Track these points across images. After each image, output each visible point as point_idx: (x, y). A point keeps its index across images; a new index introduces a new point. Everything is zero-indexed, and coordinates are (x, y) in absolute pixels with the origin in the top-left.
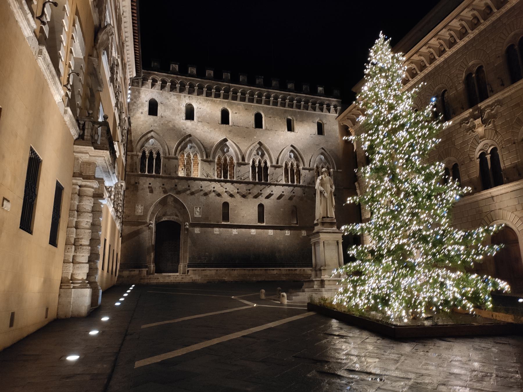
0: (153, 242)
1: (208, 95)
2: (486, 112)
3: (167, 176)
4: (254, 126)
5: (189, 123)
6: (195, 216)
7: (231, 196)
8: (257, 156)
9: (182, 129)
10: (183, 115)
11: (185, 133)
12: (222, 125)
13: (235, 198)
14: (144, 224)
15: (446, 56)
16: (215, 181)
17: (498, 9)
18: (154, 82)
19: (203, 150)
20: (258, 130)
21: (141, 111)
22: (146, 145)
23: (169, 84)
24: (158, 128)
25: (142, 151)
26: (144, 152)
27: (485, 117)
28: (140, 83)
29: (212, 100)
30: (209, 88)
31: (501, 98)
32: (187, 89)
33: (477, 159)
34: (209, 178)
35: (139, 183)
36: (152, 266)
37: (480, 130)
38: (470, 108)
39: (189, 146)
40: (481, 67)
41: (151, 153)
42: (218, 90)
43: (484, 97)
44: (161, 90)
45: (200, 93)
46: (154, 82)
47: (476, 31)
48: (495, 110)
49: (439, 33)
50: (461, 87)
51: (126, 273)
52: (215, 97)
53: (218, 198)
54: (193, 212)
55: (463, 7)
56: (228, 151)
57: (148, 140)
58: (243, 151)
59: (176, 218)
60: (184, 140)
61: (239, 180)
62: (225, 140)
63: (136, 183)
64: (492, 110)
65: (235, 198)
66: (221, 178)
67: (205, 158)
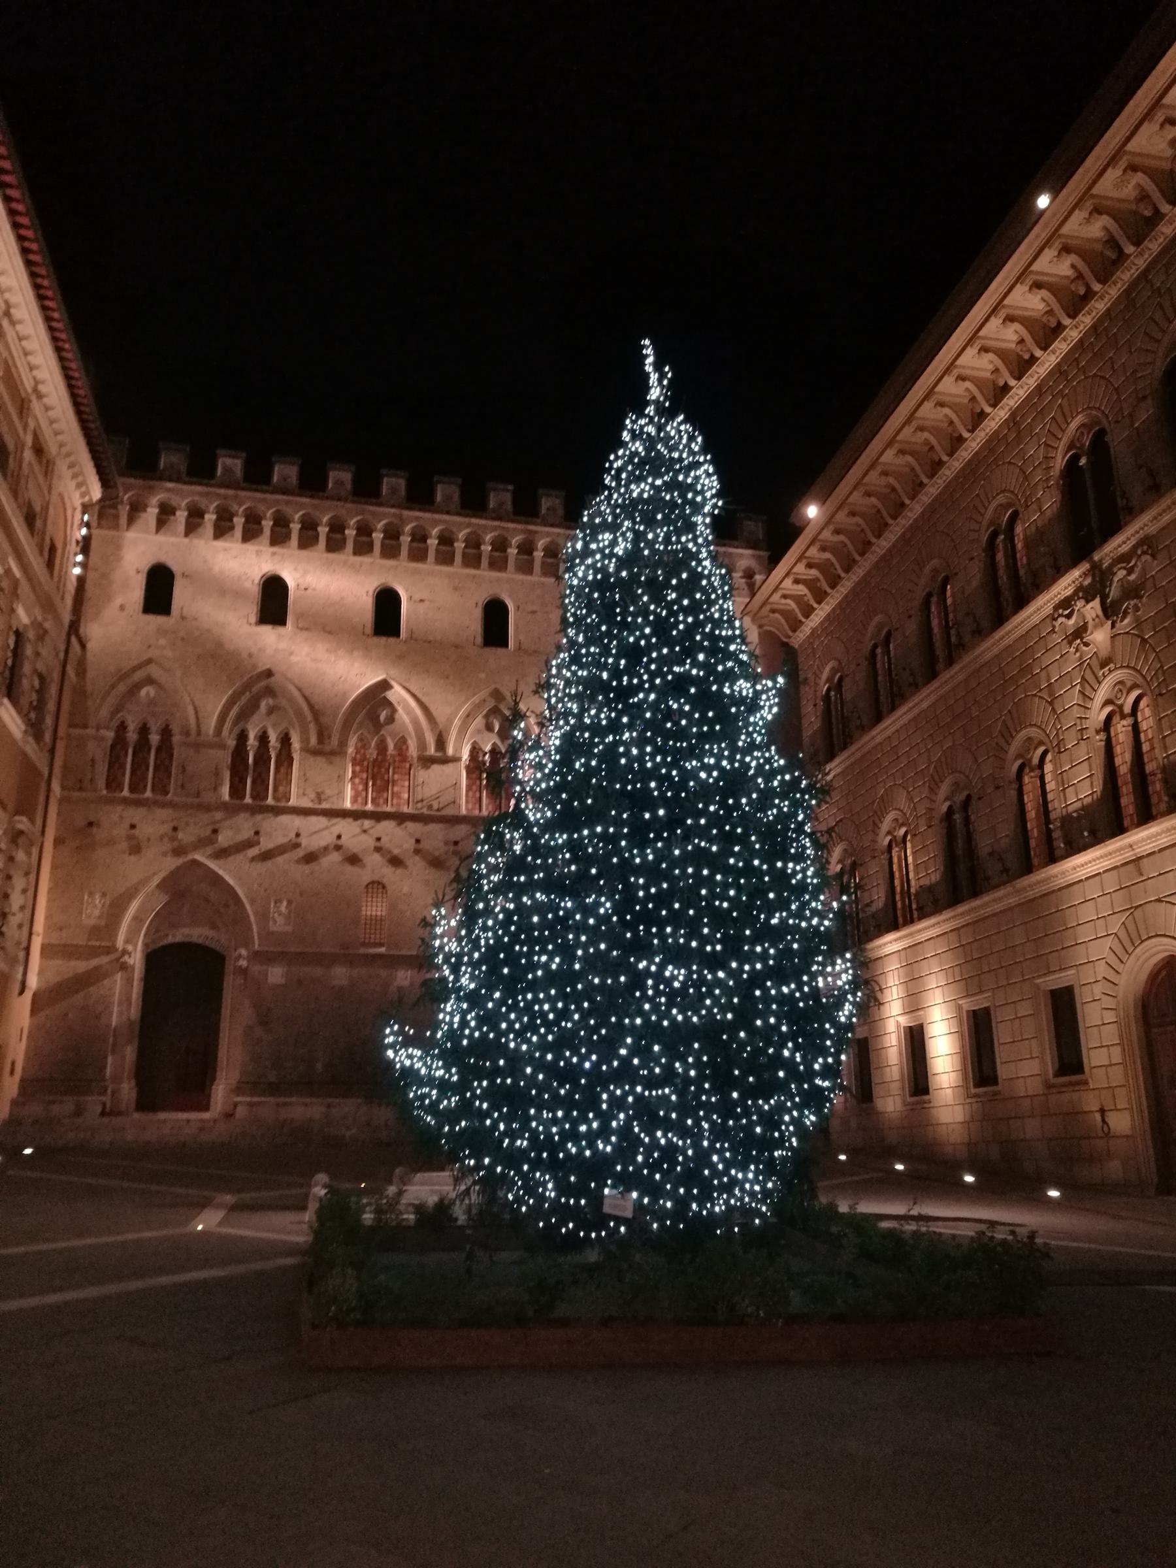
0: (135, 1012)
1: (334, 546)
2: (1116, 579)
3: (190, 800)
4: (479, 640)
5: (269, 636)
6: (273, 928)
7: (396, 862)
8: (487, 734)
9: (245, 655)
10: (252, 611)
11: (254, 666)
12: (376, 640)
13: (406, 867)
14: (108, 953)
15: (1011, 402)
16: (344, 814)
17: (1137, 244)
18: (166, 512)
19: (309, 717)
20: (490, 651)
21: (119, 601)
22: (129, 706)
23: (210, 518)
24: (168, 653)
25: (115, 723)
26: (122, 727)
27: (1114, 592)
28: (123, 520)
29: (345, 563)
30: (337, 528)
31: (1152, 529)
32: (267, 532)
33: (1098, 732)
34: (325, 805)
35: (99, 826)
36: (128, 1091)
37: (1100, 637)
38: (1074, 564)
39: (263, 705)
40: (1102, 433)
41: (144, 730)
42: (364, 530)
43: (1111, 528)
44: (186, 535)
45: (307, 542)
46: (166, 512)
47: (1086, 321)
48: (1137, 570)
49: (981, 333)
50: (1051, 502)
51: (35, 1109)
52: (355, 553)
53: (349, 868)
54: (264, 916)
55: (1036, 246)
56: (391, 719)
57: (137, 687)
58: (441, 719)
59: (210, 933)
60: (247, 687)
61: (425, 811)
62: (384, 685)
63: (91, 824)
64: (1130, 571)
65: (406, 867)
66: (366, 803)
67: (313, 740)
